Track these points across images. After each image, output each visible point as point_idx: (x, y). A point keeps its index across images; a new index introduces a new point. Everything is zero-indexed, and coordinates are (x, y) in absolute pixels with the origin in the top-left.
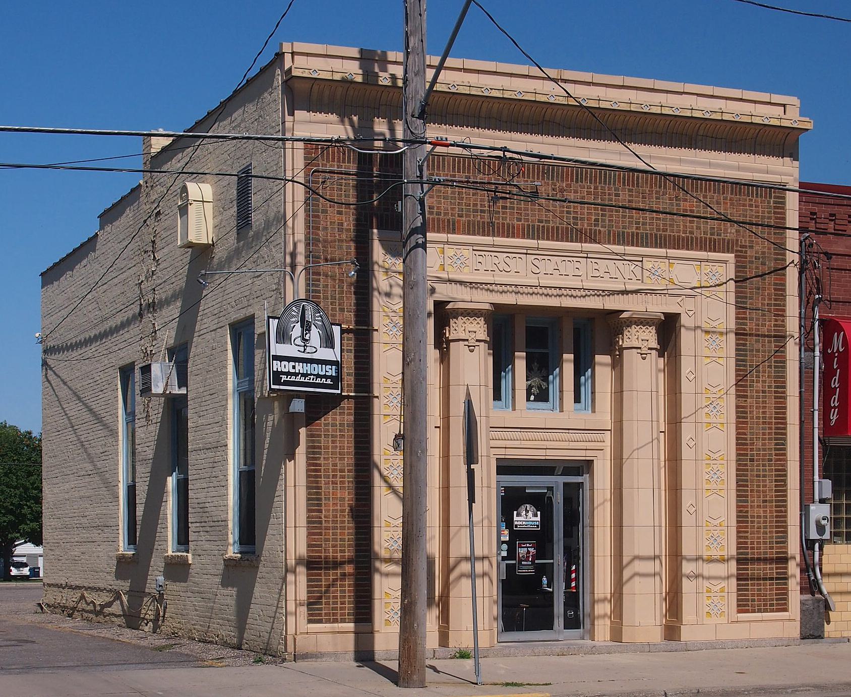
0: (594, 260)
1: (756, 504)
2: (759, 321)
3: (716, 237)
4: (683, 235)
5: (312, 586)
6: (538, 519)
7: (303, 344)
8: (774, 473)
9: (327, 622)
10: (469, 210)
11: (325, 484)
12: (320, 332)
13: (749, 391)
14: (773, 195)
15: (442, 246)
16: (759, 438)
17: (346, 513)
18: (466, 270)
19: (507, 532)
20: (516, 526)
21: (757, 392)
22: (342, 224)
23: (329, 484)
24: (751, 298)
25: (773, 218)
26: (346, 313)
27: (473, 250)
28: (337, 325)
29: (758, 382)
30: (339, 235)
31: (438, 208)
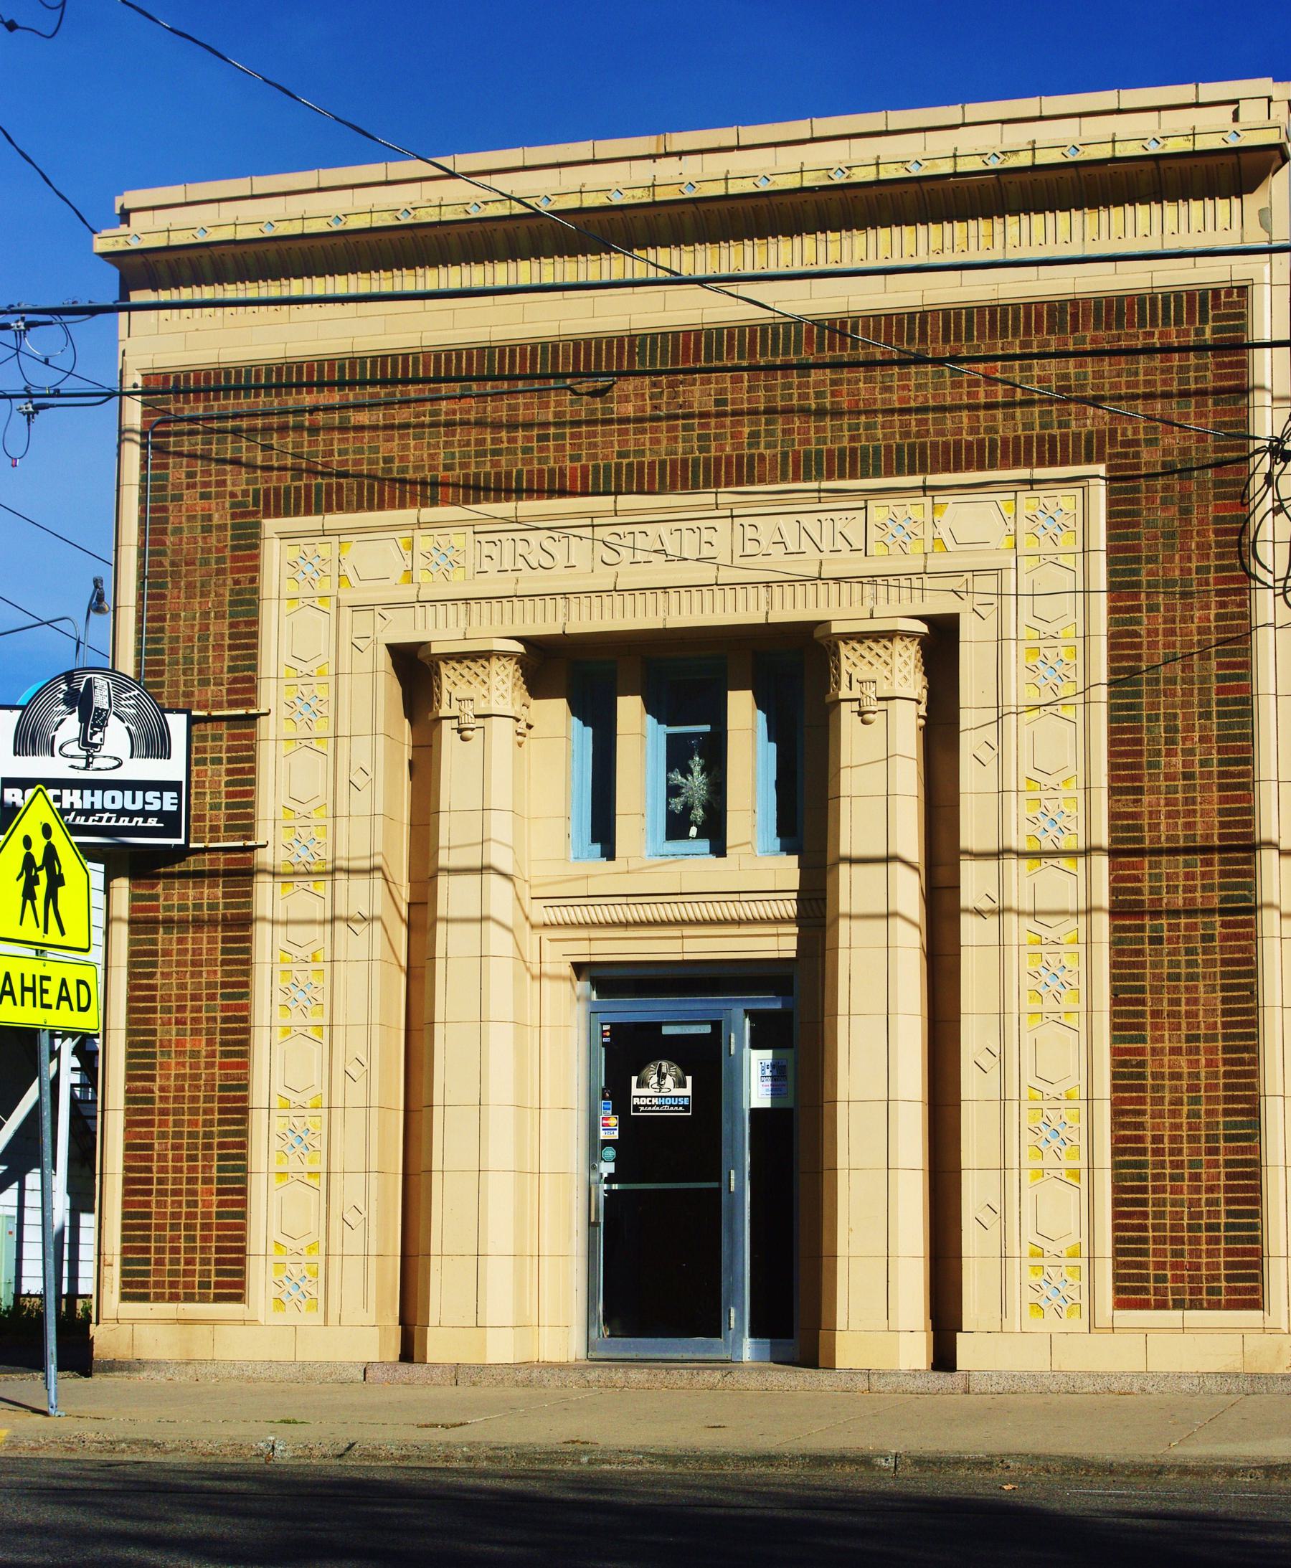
0: (746, 521)
1: (1167, 1045)
2: (1174, 610)
3: (1056, 431)
4: (970, 438)
5: (133, 1227)
6: (688, 1091)
7: (84, 753)
8: (1218, 969)
9: (159, 1298)
10: (465, 455)
11: (163, 1024)
12: (133, 728)
13: (1146, 779)
14: (1211, 313)
15: (409, 533)
16: (1177, 887)
17: (202, 1082)
18: (457, 575)
19: (614, 1121)
20: (636, 1108)
21: (1169, 777)
22: (210, 518)
23: (170, 1024)
24: (1150, 560)
25: (1211, 367)
26: (212, 687)
27: (474, 533)
28: (179, 711)
29: (1170, 753)
30: (204, 538)
31: (402, 459)
